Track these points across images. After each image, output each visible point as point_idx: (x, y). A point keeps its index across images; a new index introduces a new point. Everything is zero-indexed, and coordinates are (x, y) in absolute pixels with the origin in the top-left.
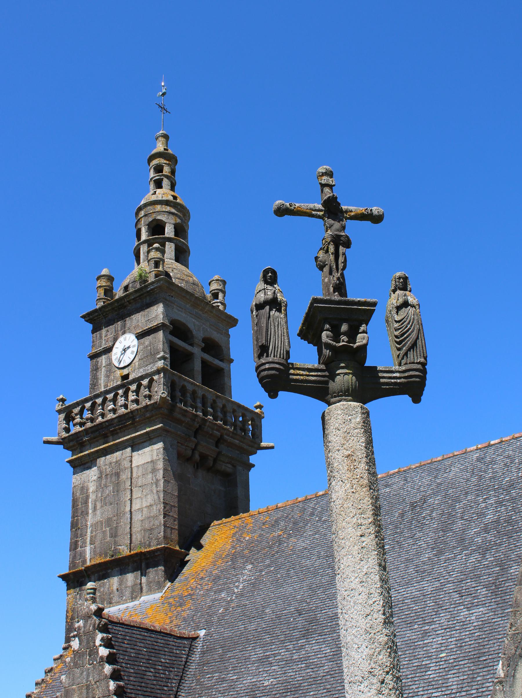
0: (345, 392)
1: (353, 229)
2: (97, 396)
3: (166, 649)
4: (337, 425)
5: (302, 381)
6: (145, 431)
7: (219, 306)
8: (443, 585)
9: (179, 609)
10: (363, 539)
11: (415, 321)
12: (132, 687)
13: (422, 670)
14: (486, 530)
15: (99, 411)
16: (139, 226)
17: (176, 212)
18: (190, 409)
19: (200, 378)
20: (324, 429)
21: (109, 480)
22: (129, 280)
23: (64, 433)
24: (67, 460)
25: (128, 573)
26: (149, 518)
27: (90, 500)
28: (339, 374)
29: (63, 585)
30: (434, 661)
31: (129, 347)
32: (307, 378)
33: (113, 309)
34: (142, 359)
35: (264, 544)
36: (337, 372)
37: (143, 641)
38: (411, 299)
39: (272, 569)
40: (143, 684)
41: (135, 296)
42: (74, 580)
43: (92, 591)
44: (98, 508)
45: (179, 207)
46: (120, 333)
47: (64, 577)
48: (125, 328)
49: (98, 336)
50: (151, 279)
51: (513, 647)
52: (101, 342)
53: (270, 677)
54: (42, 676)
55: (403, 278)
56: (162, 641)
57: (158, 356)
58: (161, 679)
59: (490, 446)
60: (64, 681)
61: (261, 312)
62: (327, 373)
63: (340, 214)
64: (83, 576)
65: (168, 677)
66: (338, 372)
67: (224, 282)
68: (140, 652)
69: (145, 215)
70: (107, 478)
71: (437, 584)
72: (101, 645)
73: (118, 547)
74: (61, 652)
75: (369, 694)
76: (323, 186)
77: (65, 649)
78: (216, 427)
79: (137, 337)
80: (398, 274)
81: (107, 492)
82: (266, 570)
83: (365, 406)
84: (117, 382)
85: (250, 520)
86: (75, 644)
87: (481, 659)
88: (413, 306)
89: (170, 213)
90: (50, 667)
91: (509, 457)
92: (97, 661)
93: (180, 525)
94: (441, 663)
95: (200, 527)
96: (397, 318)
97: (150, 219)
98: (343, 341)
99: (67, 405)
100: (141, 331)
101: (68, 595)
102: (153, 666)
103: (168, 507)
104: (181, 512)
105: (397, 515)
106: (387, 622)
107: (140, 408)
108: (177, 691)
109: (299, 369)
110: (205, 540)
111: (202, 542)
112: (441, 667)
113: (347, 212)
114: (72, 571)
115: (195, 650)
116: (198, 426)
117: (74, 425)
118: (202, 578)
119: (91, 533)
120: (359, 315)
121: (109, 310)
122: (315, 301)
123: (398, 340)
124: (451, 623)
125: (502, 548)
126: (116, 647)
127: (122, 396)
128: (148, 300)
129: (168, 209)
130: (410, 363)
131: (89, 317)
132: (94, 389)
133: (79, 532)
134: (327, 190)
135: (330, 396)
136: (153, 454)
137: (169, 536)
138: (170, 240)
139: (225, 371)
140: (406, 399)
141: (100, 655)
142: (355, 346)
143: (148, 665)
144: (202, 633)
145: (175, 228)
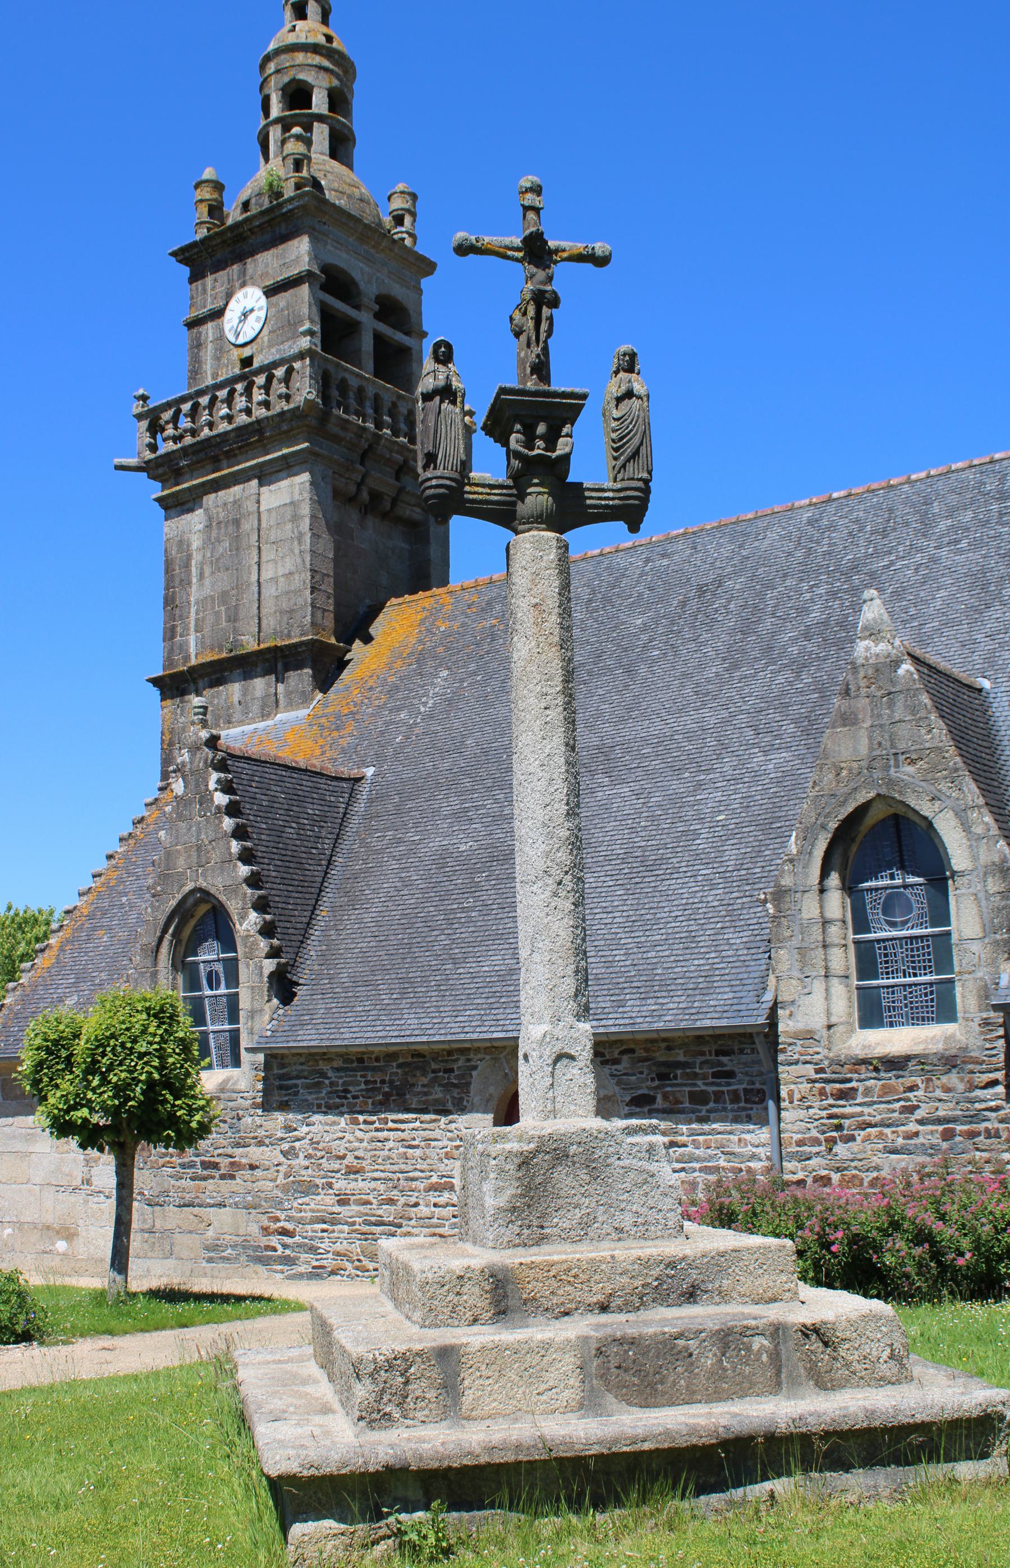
0: (538, 517)
1: (565, 278)
2: (201, 393)
3: (315, 796)
4: (524, 563)
5: (481, 502)
6: (280, 454)
7: (403, 239)
8: (733, 715)
9: (335, 734)
10: (548, 712)
11: (640, 420)
12: (264, 849)
13: (688, 838)
14: (807, 636)
15: (205, 417)
16: (266, 91)
17: (331, 66)
18: (353, 418)
19: (369, 363)
20: (508, 565)
21: (223, 531)
22: (250, 191)
23: (148, 452)
24: (154, 496)
25: (256, 677)
26: (287, 593)
27: (193, 562)
28: (530, 494)
29: (155, 693)
30: (707, 825)
31: (252, 310)
32: (487, 497)
33: (224, 242)
34: (274, 331)
35: (468, 638)
36: (529, 491)
37: (280, 783)
38: (638, 388)
39: (479, 678)
40: (281, 845)
41: (261, 221)
42: (173, 686)
43: (201, 710)
44: (206, 575)
45: (336, 57)
46: (237, 285)
47: (155, 682)
48: (244, 276)
49: (200, 288)
50: (289, 192)
51: (813, 814)
52: (205, 300)
53: (469, 840)
54: (130, 829)
55: (629, 355)
56: (309, 784)
57: (301, 329)
58: (308, 838)
59: (830, 500)
60: (163, 839)
61: (428, 404)
62: (514, 491)
63: (546, 257)
64: (187, 681)
65: (318, 835)
66: (529, 491)
67: (414, 197)
68: (276, 800)
69: (278, 71)
70: (219, 528)
71: (725, 714)
72: (216, 790)
73: (240, 638)
74: (157, 794)
75: (543, 896)
76: (526, 209)
77: (161, 789)
78: (396, 448)
79: (265, 293)
80: (623, 348)
81: (221, 550)
82: (470, 680)
83: (563, 537)
84: (233, 368)
85: (448, 599)
86: (178, 787)
87: (774, 826)
88: (639, 397)
89: (321, 68)
90: (141, 816)
91: (857, 521)
92: (211, 812)
93: (337, 604)
94: (717, 829)
95: (369, 607)
96: (616, 414)
97: (286, 79)
98: (538, 448)
99: (151, 406)
100: (272, 282)
101: (163, 708)
102: (296, 820)
103: (318, 577)
104: (339, 585)
105: (675, 603)
106: (572, 813)
107: (272, 416)
108: (331, 856)
109: (477, 485)
110: (375, 629)
111: (372, 631)
112: (716, 834)
113: (557, 251)
114: (168, 672)
115: (358, 796)
116: (366, 446)
117: (165, 440)
118: (371, 689)
119: (197, 614)
120: (562, 412)
121: (216, 245)
122: (503, 391)
123: (615, 446)
124: (737, 772)
125: (827, 666)
126: (239, 793)
127: (241, 395)
128: (283, 229)
129: (318, 60)
130: (628, 479)
131: (185, 255)
132: (195, 379)
133: (177, 612)
134: (531, 215)
135: (517, 522)
136: (289, 497)
137: (320, 622)
138: (320, 118)
139: (414, 352)
140: (621, 526)
141: (216, 803)
142: (554, 455)
143: (288, 818)
144: (370, 772)
145: (329, 96)
